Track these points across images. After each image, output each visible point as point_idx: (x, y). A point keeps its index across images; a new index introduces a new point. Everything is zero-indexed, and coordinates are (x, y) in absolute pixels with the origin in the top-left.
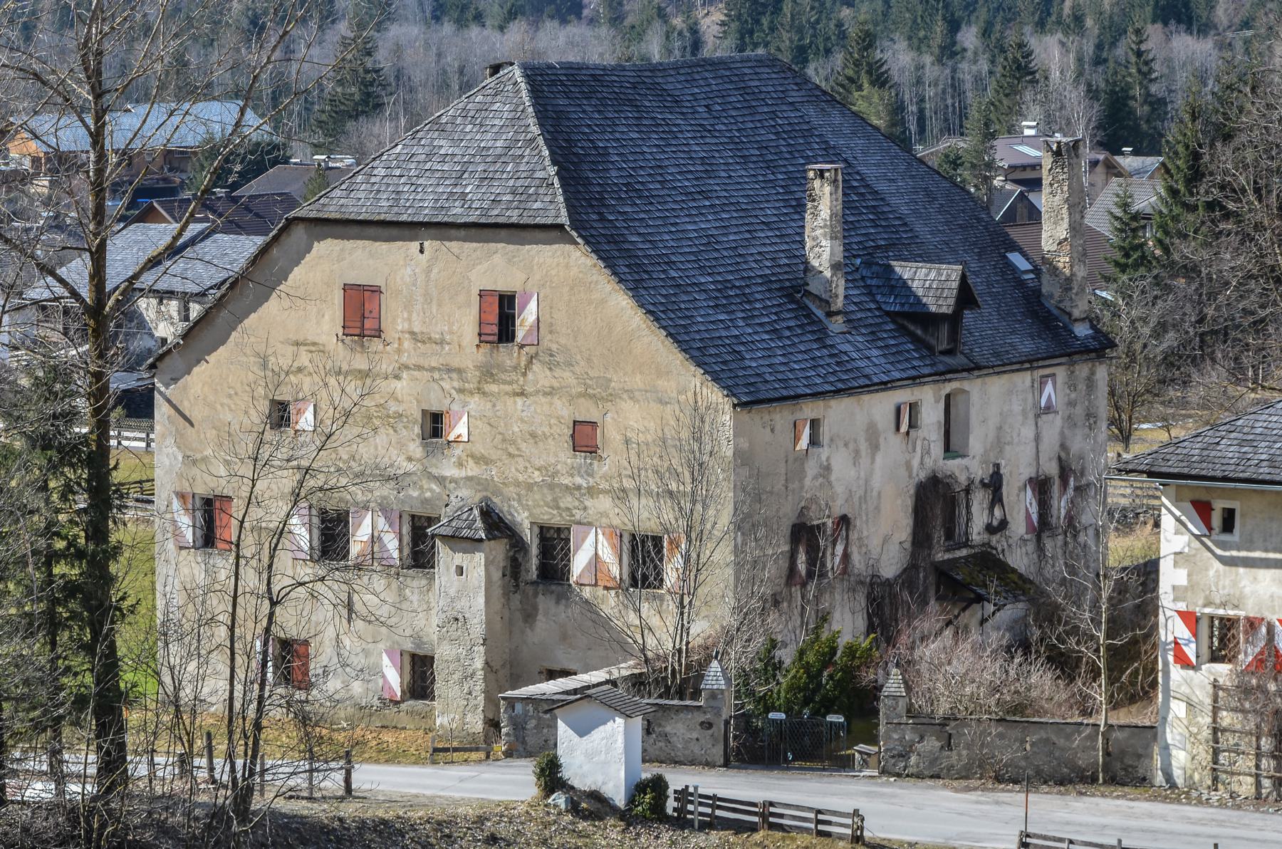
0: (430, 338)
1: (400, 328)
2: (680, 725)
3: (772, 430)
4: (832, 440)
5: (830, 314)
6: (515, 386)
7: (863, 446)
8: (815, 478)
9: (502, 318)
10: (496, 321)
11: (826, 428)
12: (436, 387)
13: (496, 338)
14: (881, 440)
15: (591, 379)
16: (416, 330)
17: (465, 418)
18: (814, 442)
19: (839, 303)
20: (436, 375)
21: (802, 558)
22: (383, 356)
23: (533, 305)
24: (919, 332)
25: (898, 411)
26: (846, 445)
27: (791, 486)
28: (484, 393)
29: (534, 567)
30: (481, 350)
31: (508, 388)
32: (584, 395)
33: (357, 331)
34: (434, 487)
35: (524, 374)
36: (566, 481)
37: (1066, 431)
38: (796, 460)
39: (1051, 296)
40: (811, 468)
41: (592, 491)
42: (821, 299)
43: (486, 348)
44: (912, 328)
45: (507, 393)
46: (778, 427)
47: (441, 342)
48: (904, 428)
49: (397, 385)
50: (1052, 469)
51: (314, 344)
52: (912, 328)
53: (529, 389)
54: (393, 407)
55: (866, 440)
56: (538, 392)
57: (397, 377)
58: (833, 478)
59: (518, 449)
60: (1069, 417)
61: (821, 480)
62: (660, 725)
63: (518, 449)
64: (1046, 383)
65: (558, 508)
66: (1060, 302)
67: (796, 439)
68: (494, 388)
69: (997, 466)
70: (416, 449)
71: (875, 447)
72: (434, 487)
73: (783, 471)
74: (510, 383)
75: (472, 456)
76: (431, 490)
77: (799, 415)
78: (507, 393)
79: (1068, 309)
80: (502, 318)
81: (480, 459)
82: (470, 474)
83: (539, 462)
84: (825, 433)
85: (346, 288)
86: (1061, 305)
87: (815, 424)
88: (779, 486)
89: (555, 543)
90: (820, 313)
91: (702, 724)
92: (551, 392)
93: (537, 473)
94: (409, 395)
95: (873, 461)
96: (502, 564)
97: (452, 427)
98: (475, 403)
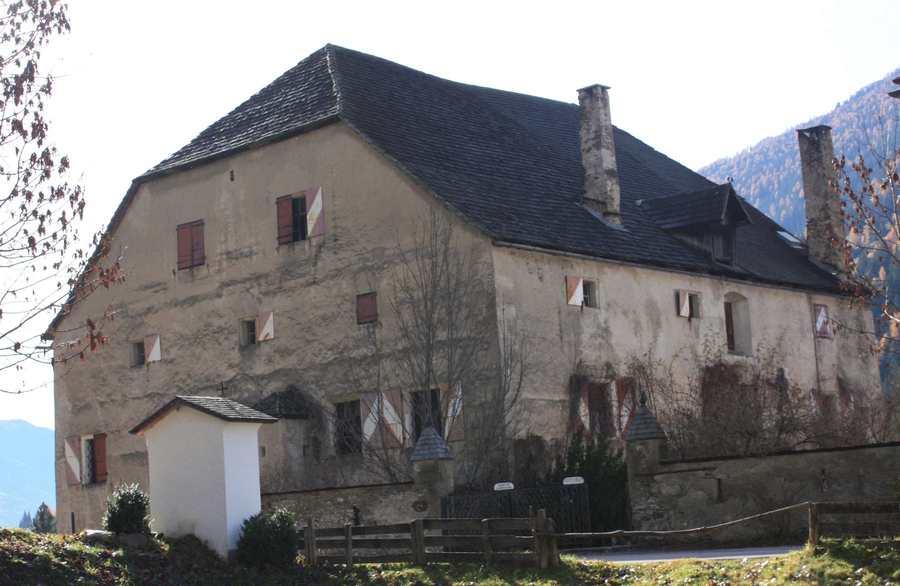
0: (241, 254)
1: (219, 251)
2: (390, 510)
3: (541, 278)
4: (609, 305)
5: (607, 214)
6: (308, 277)
7: (644, 319)
8: (593, 336)
9: (293, 220)
10: (291, 223)
11: (602, 294)
12: (248, 296)
13: (290, 238)
14: (663, 319)
15: (368, 252)
16: (231, 249)
17: (271, 318)
18: (589, 301)
19: (616, 205)
20: (248, 285)
21: (583, 410)
22: (209, 278)
23: (318, 199)
24: (696, 243)
25: (677, 297)
26: (625, 313)
27: (566, 338)
28: (284, 291)
29: (332, 443)
30: (281, 252)
31: (302, 280)
32: (363, 269)
33: (189, 264)
34: (250, 386)
35: (315, 264)
36: (355, 354)
37: (842, 358)
38: (570, 314)
39: (818, 254)
40: (588, 329)
41: (377, 358)
42: (598, 202)
43: (284, 249)
44: (689, 240)
45: (302, 286)
46: (547, 277)
47: (251, 254)
48: (685, 311)
49: (219, 302)
50: (830, 387)
51: (159, 284)
52: (689, 240)
53: (319, 277)
54: (217, 322)
55: (647, 315)
56: (326, 277)
57: (219, 296)
58: (613, 341)
59: (314, 335)
60: (843, 346)
61: (600, 340)
62: (368, 512)
63: (314, 335)
64: (819, 311)
65: (348, 381)
66: (825, 258)
67: (569, 294)
68: (292, 283)
69: (781, 371)
70: (235, 356)
71: (657, 324)
72: (250, 386)
73: (556, 321)
74: (303, 276)
75: (278, 351)
76: (248, 390)
77: (570, 273)
78: (302, 286)
79: (834, 262)
80: (293, 220)
81: (284, 352)
82: (277, 367)
83: (330, 342)
84: (601, 295)
85: (180, 228)
86: (827, 261)
87: (588, 288)
88: (553, 334)
89: (349, 413)
90: (598, 215)
91: (415, 505)
92: (337, 274)
93: (330, 353)
94: (227, 309)
95: (655, 337)
96: (302, 444)
97: (261, 328)
98: (279, 302)
